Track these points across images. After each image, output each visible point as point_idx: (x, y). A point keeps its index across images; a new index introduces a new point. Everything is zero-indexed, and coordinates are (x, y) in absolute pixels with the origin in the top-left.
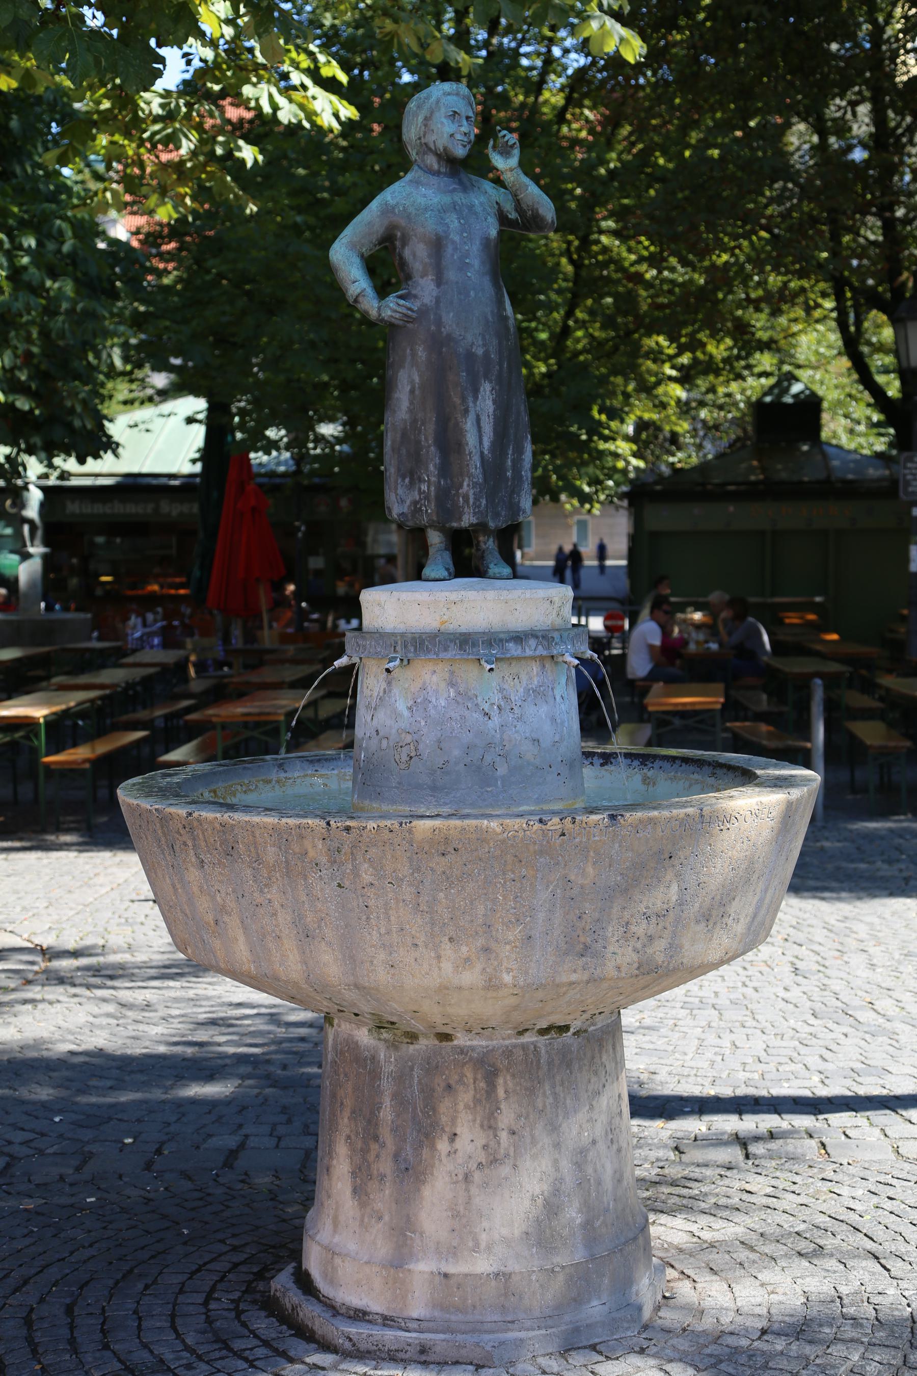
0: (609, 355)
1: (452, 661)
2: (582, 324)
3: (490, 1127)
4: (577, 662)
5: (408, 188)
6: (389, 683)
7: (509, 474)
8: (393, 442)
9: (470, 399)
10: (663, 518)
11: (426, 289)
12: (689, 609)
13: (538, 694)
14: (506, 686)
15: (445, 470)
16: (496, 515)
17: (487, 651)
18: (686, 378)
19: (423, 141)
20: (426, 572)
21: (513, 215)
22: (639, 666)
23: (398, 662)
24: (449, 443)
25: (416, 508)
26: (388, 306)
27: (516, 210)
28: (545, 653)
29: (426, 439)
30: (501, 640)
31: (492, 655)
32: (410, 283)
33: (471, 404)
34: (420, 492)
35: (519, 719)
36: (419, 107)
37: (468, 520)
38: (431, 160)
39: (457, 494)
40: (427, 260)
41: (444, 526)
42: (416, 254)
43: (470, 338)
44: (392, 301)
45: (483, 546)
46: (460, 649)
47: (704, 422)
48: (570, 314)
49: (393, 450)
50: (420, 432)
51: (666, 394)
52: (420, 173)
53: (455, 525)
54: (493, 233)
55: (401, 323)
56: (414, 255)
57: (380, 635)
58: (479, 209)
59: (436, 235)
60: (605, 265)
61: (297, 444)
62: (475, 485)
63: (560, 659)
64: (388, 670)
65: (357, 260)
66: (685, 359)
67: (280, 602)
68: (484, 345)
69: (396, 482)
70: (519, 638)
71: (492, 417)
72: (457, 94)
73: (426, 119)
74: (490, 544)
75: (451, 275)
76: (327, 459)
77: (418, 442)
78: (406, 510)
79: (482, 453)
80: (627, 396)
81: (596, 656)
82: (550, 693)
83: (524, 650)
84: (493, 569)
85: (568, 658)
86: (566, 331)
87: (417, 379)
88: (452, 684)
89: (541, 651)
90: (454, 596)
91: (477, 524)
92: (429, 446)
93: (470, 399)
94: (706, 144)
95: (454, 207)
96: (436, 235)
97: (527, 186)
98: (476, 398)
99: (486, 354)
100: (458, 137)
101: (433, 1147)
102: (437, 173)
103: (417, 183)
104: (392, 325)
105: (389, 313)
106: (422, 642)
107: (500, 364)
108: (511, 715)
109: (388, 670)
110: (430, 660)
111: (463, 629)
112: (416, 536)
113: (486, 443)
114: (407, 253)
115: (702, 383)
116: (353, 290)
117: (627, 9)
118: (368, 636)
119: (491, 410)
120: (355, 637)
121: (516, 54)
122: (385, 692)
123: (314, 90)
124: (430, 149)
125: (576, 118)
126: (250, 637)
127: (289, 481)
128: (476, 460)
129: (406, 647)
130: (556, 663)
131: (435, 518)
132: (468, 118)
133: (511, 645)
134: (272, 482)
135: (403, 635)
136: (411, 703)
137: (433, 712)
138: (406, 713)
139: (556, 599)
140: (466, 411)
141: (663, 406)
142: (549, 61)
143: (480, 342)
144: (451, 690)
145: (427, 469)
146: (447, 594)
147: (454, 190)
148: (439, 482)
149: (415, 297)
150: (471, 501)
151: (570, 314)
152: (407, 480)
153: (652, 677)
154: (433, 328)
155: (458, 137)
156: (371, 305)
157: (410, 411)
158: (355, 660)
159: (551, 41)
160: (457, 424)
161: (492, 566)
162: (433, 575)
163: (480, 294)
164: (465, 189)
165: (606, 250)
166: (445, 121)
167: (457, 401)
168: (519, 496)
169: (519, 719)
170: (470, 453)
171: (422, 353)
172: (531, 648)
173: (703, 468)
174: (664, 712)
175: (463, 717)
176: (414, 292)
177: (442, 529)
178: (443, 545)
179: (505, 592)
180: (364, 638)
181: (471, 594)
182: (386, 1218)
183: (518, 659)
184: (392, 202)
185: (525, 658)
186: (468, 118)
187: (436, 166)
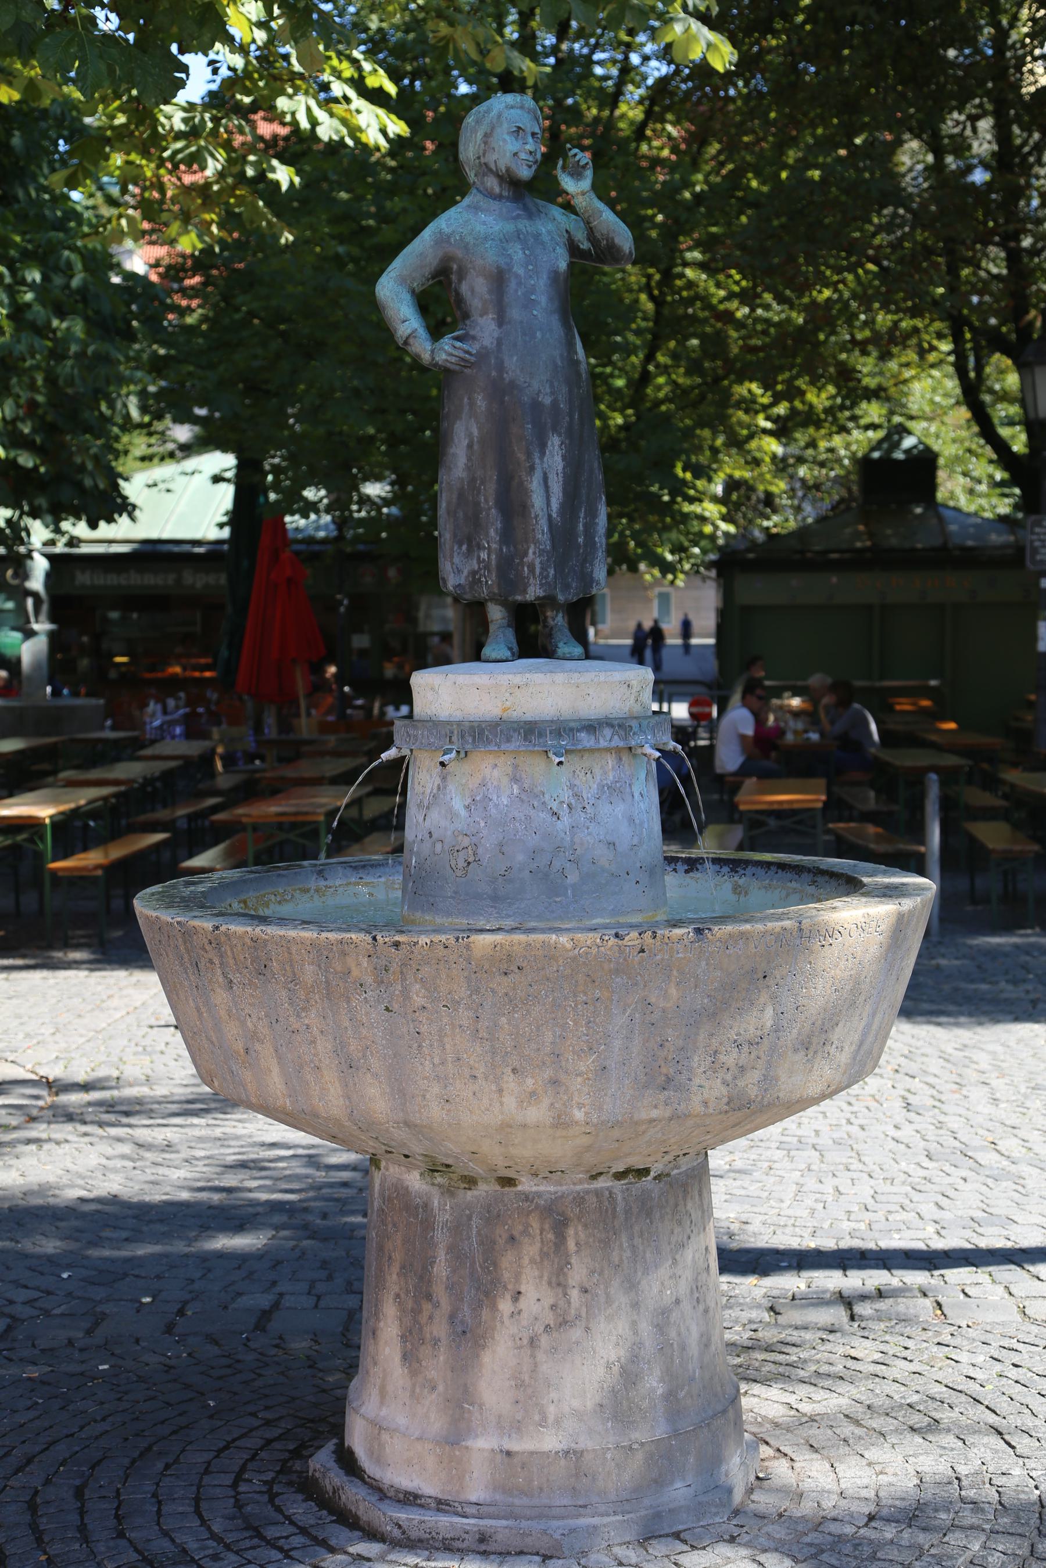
0: (695, 405)
2: (664, 370)
3: (559, 1284)
4: (658, 754)
6: (444, 779)
7: (581, 540)
8: (449, 503)
9: (537, 455)
10: (756, 590)
11: (485, 329)
12: (786, 694)
13: (614, 791)
14: (577, 782)
15: (507, 535)
16: (566, 587)
17: (555, 742)
18: (782, 430)
19: (482, 160)
20: (486, 651)
21: (585, 245)
22: (729, 758)
23: (453, 755)
24: (512, 505)
25: (475, 579)
26: (442, 349)
27: (589, 240)
28: (621, 744)
29: (486, 501)
30: (572, 730)
31: (561, 746)
32: (468, 322)
33: (537, 461)
34: (479, 561)
35: (592, 819)
36: (478, 122)
37: (533, 592)
38: (492, 183)
39: (522, 563)
40: (487, 296)
41: (506, 600)
42: (475, 289)
43: (535, 385)
44: (447, 343)
45: (551, 623)
46: (525, 739)
47: (803, 481)
48: (650, 358)
49: (448, 513)
50: (479, 492)
51: (760, 449)
52: (479, 197)
53: (519, 598)
54: (563, 265)
55: (457, 368)
56: (473, 291)
57: (433, 724)
58: (546, 238)
59: (498, 267)
60: (690, 302)
61: (338, 506)
62: (542, 552)
64: (442, 764)
65: (407, 297)
66: (781, 409)
67: (319, 686)
68: (552, 393)
69: (452, 549)
70: (592, 727)
71: (561, 475)
72: (522, 107)
74: (558, 620)
75: (515, 313)
76: (373, 523)
77: (477, 504)
78: (463, 581)
79: (550, 516)
80: (715, 451)
81: (680, 747)
83: (597, 741)
84: (563, 649)
85: (648, 750)
86: (646, 378)
87: (475, 432)
88: (515, 779)
89: (617, 742)
90: (517, 679)
91: (544, 597)
92: (489, 509)
93: (537, 455)
94: (806, 164)
95: (518, 235)
96: (498, 267)
97: (601, 212)
98: (543, 454)
99: (555, 403)
100: (523, 156)
101: (494, 1307)
102: (499, 197)
103: (475, 208)
104: (447, 371)
105: (444, 356)
106: (481, 732)
107: (571, 415)
108: (583, 815)
109: (442, 764)
110: (490, 752)
111: (528, 717)
112: (475, 611)
113: (555, 505)
114: (464, 288)
115: (801, 437)
116: (402, 331)
117: (715, 10)
118: (419, 725)
119: (560, 468)
120: (405, 726)
121: (588, 62)
123: (358, 102)
124: (491, 170)
125: (657, 134)
126: (285, 725)
127: (330, 548)
128: (543, 524)
129: (463, 737)
130: (635, 756)
131: (496, 591)
132: (533, 134)
133: (583, 735)
134: (311, 549)
135: (459, 723)
136: (469, 801)
138: (463, 813)
139: (634, 683)
140: (532, 468)
141: (757, 462)
142: (626, 69)
143: (548, 390)
144: (515, 786)
145: (487, 534)
146: (510, 677)
147: (518, 217)
148: (501, 550)
149: (474, 338)
150: (538, 571)
151: (650, 358)
152: (464, 547)
153: (744, 771)
154: (494, 373)
155: (523, 156)
156: (423, 347)
157: (468, 468)
158: (405, 752)
159: (629, 47)
160: (521, 483)
161: (561, 645)
162: (494, 655)
163: (548, 335)
164: (530, 216)
165: (691, 285)
166: (507, 137)
167: (522, 457)
168: (592, 565)
169: (592, 819)
170: (537, 516)
171: (481, 402)
172: (606, 738)
173: (802, 533)
174: (757, 812)
175: (528, 817)
176: (472, 333)
177: (504, 603)
178: (505, 621)
179: (576, 675)
180: (415, 727)
181: (538, 677)
182: (441, 1388)
183: (591, 751)
184: (447, 230)
185: (599, 750)
186: (533, 134)
187: (497, 190)
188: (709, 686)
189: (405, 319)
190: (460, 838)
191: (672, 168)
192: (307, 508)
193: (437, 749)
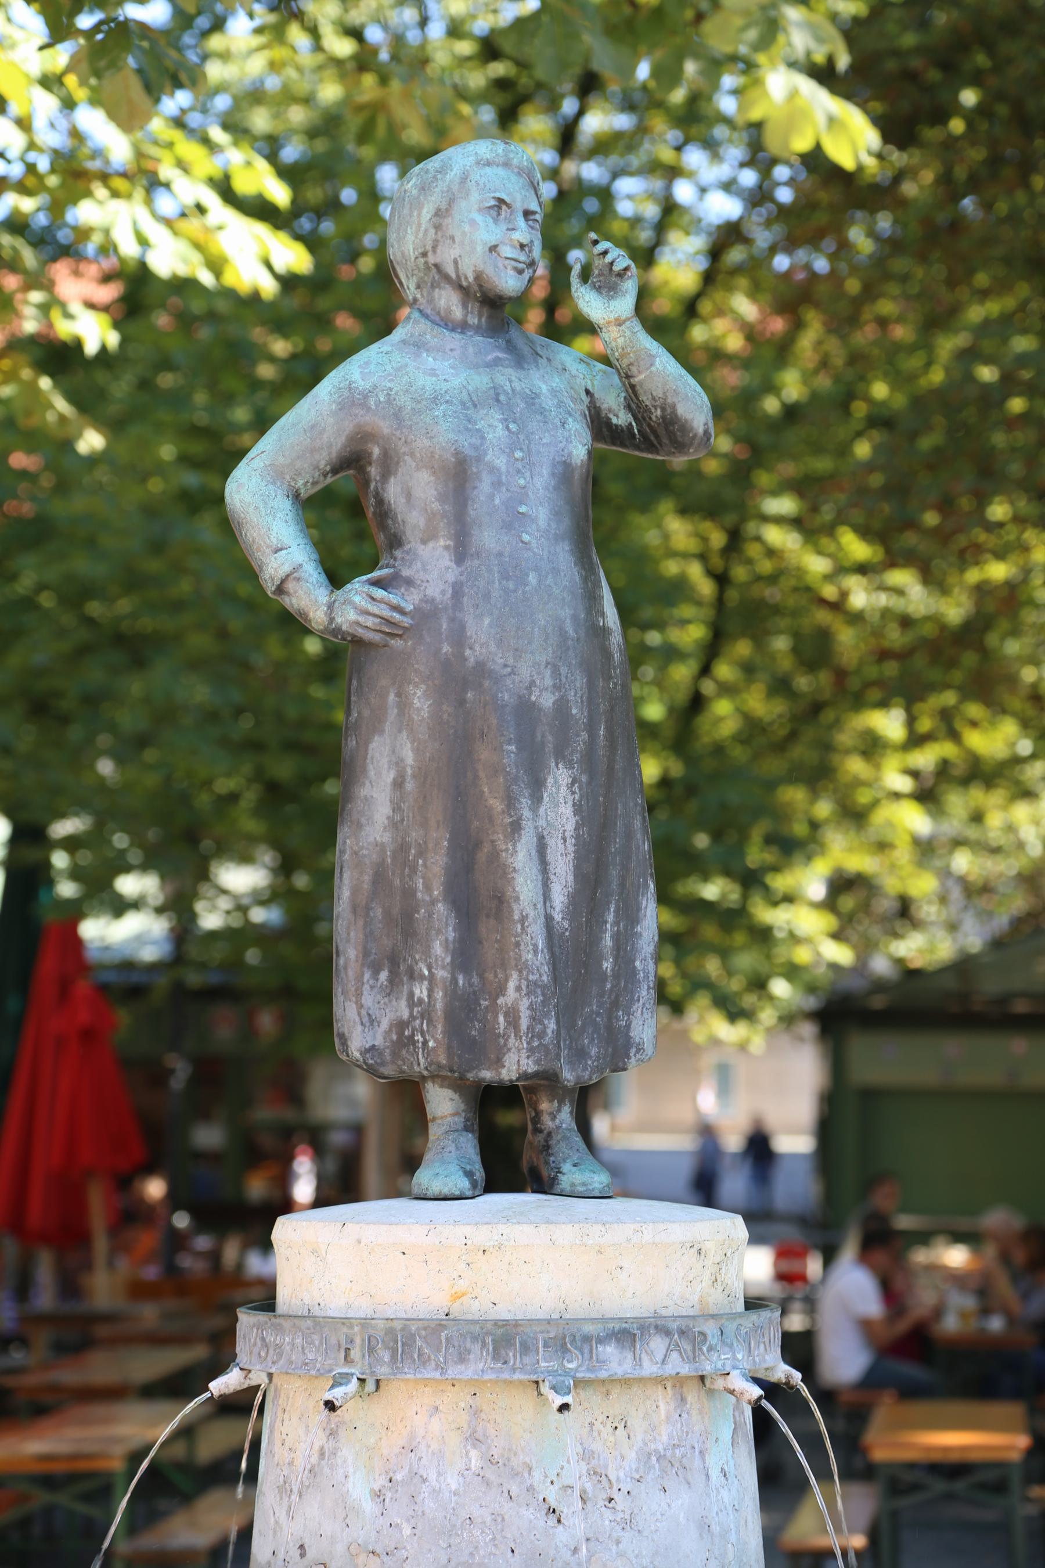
0: (781, 746)
1: (475, 1387)
2: (727, 690)
4: (757, 1392)
5: (396, 356)
6: (332, 1434)
7: (607, 965)
8: (355, 891)
9: (525, 802)
10: (888, 1061)
11: (430, 566)
12: (940, 1240)
13: (670, 1464)
14: (597, 1446)
15: (466, 955)
16: (579, 1055)
17: (554, 1365)
18: (927, 795)
19: (431, 259)
20: (425, 1178)
21: (622, 418)
22: (845, 1361)
23: (353, 1385)
24: (477, 898)
25: (403, 1038)
26: (348, 602)
27: (628, 407)
28: (685, 1370)
29: (428, 888)
30: (587, 1339)
31: (567, 1373)
32: (398, 553)
33: (526, 813)
34: (412, 1002)
35: (628, 1523)
36: (423, 189)
37: (515, 1064)
38: (449, 300)
39: (494, 1008)
40: (436, 506)
41: (462, 1078)
42: (412, 494)
43: (525, 671)
44: (358, 590)
45: (548, 1123)
46: (496, 1356)
47: (963, 881)
48: (705, 670)
49: (354, 909)
50: (414, 870)
51: (890, 824)
52: (424, 325)
53: (487, 1075)
54: (579, 451)
55: (377, 637)
56: (409, 496)
57: (314, 1323)
58: (548, 402)
59: (457, 453)
60: (773, 579)
61: (179, 908)
62: (532, 988)
63: (720, 1383)
64: (330, 1406)
65: (284, 506)
66: (925, 759)
67: (132, 1215)
68: (557, 687)
69: (359, 978)
70: (627, 1334)
71: (571, 841)
72: (507, 164)
73: (438, 213)
74: (561, 1117)
75: (488, 538)
76: (238, 936)
77: (409, 893)
78: (379, 1041)
79: (549, 919)
80: (814, 825)
81: (797, 1376)
82: (697, 1462)
83: (638, 1362)
84: (570, 1176)
85: (739, 1383)
86: (697, 703)
87: (409, 757)
88: (474, 1439)
89: (677, 1365)
90: (483, 1236)
91: (536, 1075)
92: (433, 902)
93: (525, 802)
94: (969, 356)
95: (496, 396)
96: (457, 453)
97: (652, 357)
98: (537, 800)
99: (561, 707)
100: (507, 251)
102: (462, 327)
103: (418, 345)
104: (358, 642)
105: (352, 616)
106: (409, 1342)
107: (591, 728)
108: (608, 1514)
109: (330, 1406)
110: (426, 1382)
111: (502, 1313)
112: (406, 1096)
113: (559, 897)
114: (393, 492)
115: (958, 802)
116: (273, 568)
117: (843, 61)
118: (287, 1324)
119: (570, 826)
120: (259, 1326)
121: (605, 195)
122: (322, 1454)
123: (219, 211)
124: (446, 277)
125: (720, 312)
126: (70, 1286)
127: (162, 982)
128: (537, 933)
129: (371, 1350)
130: (711, 1392)
131: (443, 1060)
132: (527, 214)
133: (609, 1350)
134: (128, 982)
135: (365, 1323)
136: (382, 1481)
137: (429, 1505)
138: (369, 1507)
139: (710, 1246)
140: (516, 827)
141: (882, 846)
142: (670, 208)
143: (549, 682)
144: (474, 1454)
145: (427, 951)
146: (468, 1230)
147: (496, 362)
148: (454, 980)
149: (409, 582)
150: (524, 1023)
151: (705, 670)
152: (384, 975)
153: (872, 1381)
154: (446, 648)
155: (507, 251)
156: (312, 598)
157: (394, 825)
158: (258, 1378)
159: (673, 172)
160: (495, 855)
161: (566, 1167)
162: (437, 1187)
163: (550, 581)
164: (520, 361)
165: (771, 552)
166: (479, 218)
167: (497, 805)
168: (628, 1013)
169: (628, 1523)
170: (523, 919)
171: (420, 701)
172: (656, 1357)
173: (963, 966)
174: (912, 1466)
175: (499, 1518)
176: (406, 573)
177: (458, 1084)
178: (460, 1120)
179: (598, 1228)
180: (279, 1329)
181: (521, 1233)
183: (626, 1382)
184: (362, 384)
185: (641, 1380)
186: (527, 214)
187: (458, 313)
188: (802, 1221)
189: (279, 545)
190: (362, 1559)
191: (744, 362)
192: (120, 907)
193: (320, 1375)
